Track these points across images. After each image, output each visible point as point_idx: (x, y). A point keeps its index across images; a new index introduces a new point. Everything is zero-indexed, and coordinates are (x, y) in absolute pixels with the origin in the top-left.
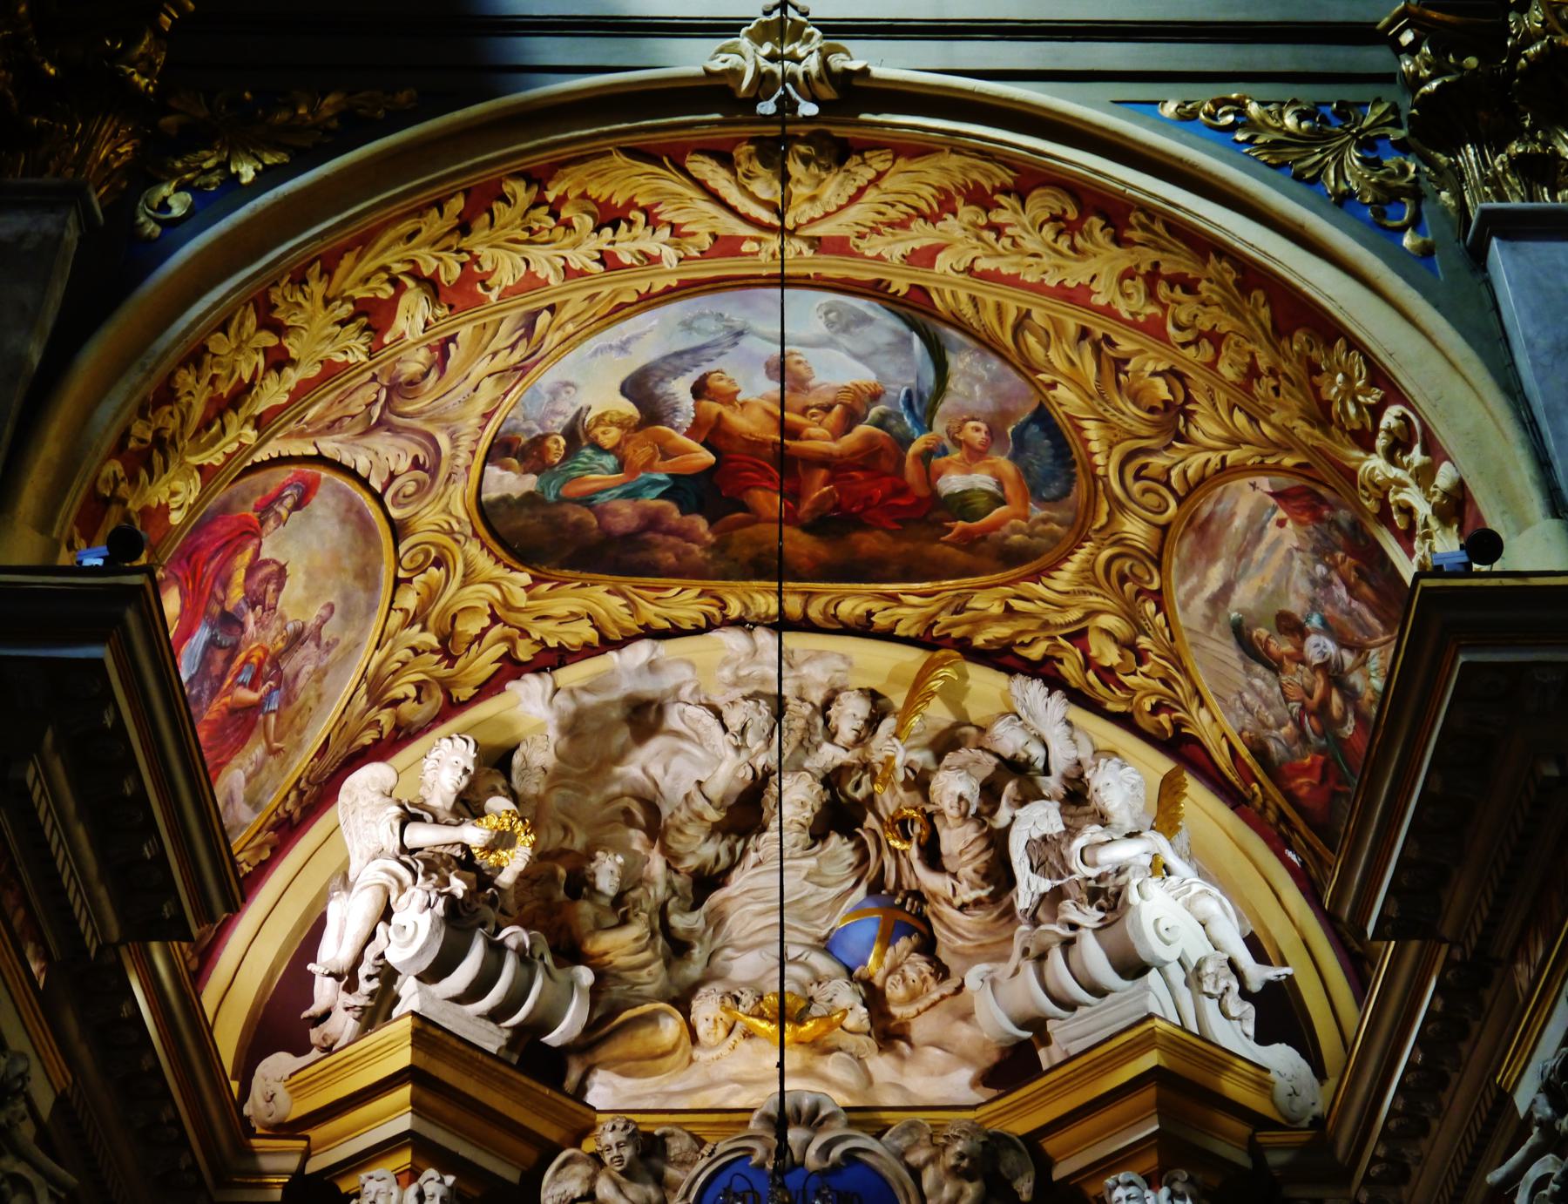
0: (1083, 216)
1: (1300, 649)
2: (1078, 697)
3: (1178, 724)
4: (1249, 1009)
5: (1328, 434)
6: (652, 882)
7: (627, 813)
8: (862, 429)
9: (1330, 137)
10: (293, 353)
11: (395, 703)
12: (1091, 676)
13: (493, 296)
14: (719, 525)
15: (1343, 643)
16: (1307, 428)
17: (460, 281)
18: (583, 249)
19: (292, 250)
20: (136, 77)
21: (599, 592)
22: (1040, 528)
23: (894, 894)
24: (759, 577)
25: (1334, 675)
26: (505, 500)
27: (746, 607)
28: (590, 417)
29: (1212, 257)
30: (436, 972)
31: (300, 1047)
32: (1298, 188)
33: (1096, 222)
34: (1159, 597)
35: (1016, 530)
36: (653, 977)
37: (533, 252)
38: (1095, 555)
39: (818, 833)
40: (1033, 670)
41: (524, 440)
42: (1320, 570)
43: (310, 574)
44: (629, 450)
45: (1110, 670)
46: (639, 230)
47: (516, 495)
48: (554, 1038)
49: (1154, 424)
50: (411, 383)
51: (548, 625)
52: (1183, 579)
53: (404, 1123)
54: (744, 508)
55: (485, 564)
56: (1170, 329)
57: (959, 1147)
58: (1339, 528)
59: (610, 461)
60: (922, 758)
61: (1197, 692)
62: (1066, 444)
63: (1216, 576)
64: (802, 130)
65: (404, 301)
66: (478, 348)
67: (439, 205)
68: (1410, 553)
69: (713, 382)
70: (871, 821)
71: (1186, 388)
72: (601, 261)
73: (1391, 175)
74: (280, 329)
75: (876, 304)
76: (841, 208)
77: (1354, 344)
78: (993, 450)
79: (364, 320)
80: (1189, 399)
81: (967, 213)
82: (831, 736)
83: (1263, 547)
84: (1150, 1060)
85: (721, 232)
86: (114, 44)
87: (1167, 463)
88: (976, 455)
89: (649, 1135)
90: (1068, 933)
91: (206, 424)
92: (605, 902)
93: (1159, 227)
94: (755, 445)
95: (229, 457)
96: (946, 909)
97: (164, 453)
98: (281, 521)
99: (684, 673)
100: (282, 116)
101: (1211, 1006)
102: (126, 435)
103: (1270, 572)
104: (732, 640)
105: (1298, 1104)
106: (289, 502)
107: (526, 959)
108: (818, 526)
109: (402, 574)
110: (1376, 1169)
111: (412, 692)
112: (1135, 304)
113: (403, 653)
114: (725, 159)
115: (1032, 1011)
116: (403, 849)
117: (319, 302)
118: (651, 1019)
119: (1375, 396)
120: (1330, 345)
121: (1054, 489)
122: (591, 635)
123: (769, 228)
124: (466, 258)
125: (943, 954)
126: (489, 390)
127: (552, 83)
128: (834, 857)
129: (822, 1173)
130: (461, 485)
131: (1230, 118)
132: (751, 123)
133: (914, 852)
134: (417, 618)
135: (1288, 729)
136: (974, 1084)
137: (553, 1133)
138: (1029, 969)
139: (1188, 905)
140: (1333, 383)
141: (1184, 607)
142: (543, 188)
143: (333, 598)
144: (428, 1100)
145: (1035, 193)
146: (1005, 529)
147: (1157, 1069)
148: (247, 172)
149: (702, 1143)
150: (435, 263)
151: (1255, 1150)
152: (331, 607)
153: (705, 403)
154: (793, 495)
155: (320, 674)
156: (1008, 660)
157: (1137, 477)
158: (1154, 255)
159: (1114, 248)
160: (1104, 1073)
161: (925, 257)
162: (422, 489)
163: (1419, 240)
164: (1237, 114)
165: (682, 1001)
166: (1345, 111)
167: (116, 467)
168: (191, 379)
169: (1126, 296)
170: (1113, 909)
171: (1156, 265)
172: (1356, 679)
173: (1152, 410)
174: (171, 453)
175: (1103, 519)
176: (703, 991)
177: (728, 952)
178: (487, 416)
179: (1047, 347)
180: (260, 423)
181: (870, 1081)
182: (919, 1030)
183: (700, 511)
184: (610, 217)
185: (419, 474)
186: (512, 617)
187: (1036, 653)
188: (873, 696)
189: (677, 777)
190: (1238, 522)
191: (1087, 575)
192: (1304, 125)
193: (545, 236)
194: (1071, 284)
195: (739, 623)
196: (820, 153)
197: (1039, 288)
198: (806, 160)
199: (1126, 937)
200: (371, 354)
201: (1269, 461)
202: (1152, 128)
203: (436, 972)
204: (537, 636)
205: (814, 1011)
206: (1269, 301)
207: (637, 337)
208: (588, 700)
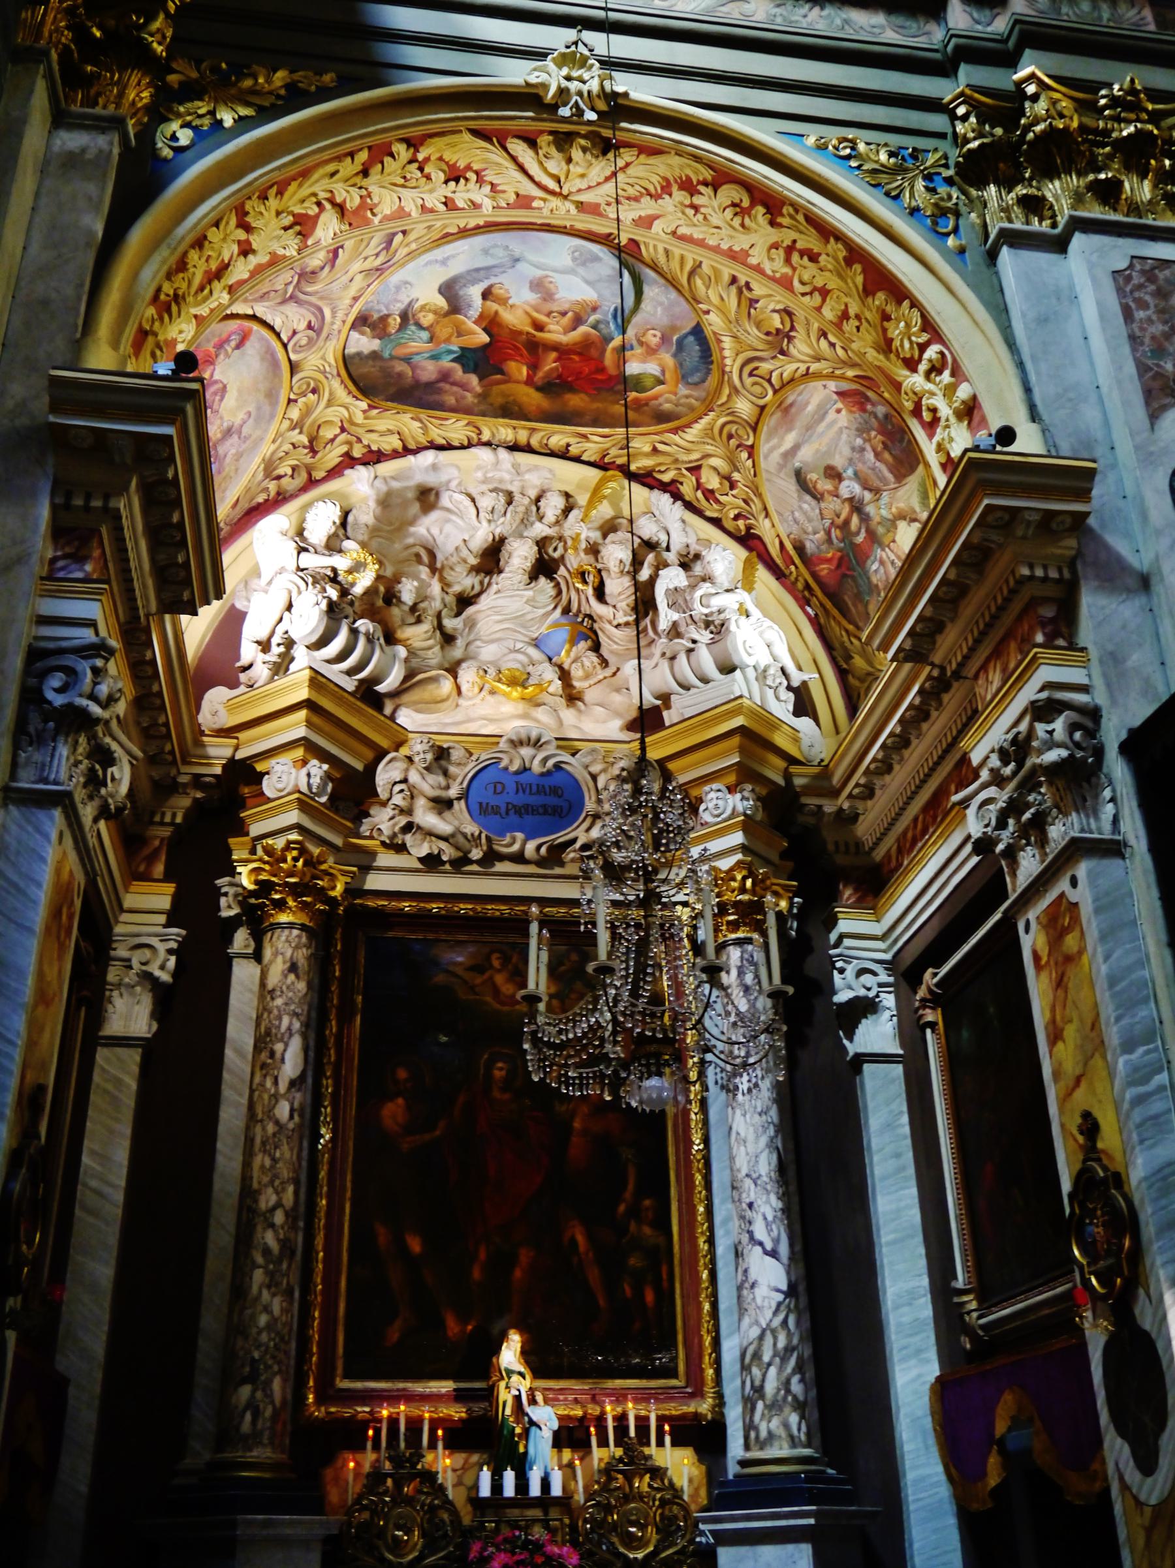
0: (753, 204)
1: (837, 488)
2: (689, 506)
3: (749, 528)
4: (791, 696)
5: (888, 359)
6: (434, 599)
7: (418, 556)
8: (583, 329)
9: (906, 170)
10: (254, 246)
11: (279, 477)
12: (699, 494)
13: (376, 220)
14: (486, 381)
15: (866, 487)
16: (875, 354)
17: (359, 207)
18: (435, 194)
19: (261, 176)
20: (155, 45)
21: (406, 418)
22: (683, 401)
23: (576, 615)
24: (504, 417)
25: (856, 506)
26: (359, 354)
27: (493, 435)
28: (417, 306)
29: (832, 240)
30: (322, 642)
31: (233, 684)
32: (888, 201)
33: (760, 210)
34: (751, 450)
35: (668, 401)
36: (434, 655)
37: (404, 193)
38: (715, 421)
39: (533, 577)
40: (664, 487)
41: (376, 316)
42: (859, 441)
43: (240, 391)
44: (437, 329)
45: (712, 492)
46: (472, 184)
47: (366, 351)
48: (382, 688)
49: (768, 343)
50: (313, 273)
51: (373, 436)
52: (768, 440)
53: (301, 732)
54: (502, 372)
55: (341, 394)
56: (796, 283)
57: (622, 764)
58: (876, 417)
59: (425, 335)
60: (595, 536)
61: (765, 509)
62: (709, 349)
63: (790, 440)
64: (583, 129)
65: (323, 218)
66: (356, 254)
67: (352, 155)
68: (931, 436)
69: (495, 291)
70: (562, 571)
71: (792, 321)
72: (445, 204)
73: (942, 199)
74: (248, 229)
75: (605, 249)
76: (599, 184)
77: (915, 304)
78: (662, 350)
79: (298, 228)
80: (792, 328)
81: (679, 196)
82: (541, 518)
83: (823, 424)
84: (739, 721)
85: (521, 192)
86: (138, 18)
87: (771, 367)
88: (651, 351)
89: (440, 748)
90: (692, 646)
91: (201, 289)
92: (406, 608)
93: (800, 218)
94: (517, 333)
95: (212, 310)
96: (608, 627)
97: (178, 304)
98: (228, 356)
99: (454, 473)
100: (248, 83)
101: (770, 693)
102: (159, 290)
103: (825, 440)
104: (484, 454)
105: (814, 751)
106: (233, 344)
107: (370, 639)
108: (548, 388)
109: (292, 396)
110: (857, 791)
111: (289, 472)
112: (776, 265)
113: (287, 447)
114: (532, 143)
115: (665, 689)
116: (299, 569)
117: (273, 213)
118: (434, 680)
119: (924, 337)
120: (899, 303)
121: (696, 378)
122: (398, 445)
123: (552, 193)
124: (364, 192)
125: (604, 651)
126: (359, 281)
128: (542, 591)
129: (542, 775)
130: (334, 342)
131: (848, 151)
132: (552, 121)
133: (590, 591)
134: (297, 425)
135: (821, 535)
136: (621, 730)
137: (384, 743)
138: (665, 665)
139: (761, 634)
140: (897, 327)
141: (766, 457)
142: (417, 151)
144: (316, 720)
145: (725, 187)
146: (661, 400)
147: (742, 727)
148: (227, 118)
149: (471, 754)
150: (345, 194)
151: (788, 776)
152: (249, 414)
153: (489, 303)
154: (534, 367)
155: (239, 456)
156: (649, 480)
157: (751, 374)
158: (793, 235)
159: (769, 227)
160: (709, 727)
161: (647, 222)
162: (311, 342)
163: (958, 243)
164: (853, 149)
165: (453, 670)
166: (916, 154)
167: (151, 311)
168: (196, 257)
169: (771, 259)
170: (719, 633)
171: (794, 241)
172: (870, 509)
173: (768, 334)
174: (183, 305)
175: (724, 399)
176: (464, 665)
177: (478, 643)
178: (356, 299)
179: (708, 288)
180: (231, 289)
181: (560, 722)
182: (589, 696)
183: (475, 371)
184: (455, 176)
185: (310, 332)
186: (353, 429)
187: (666, 478)
188: (567, 495)
189: (447, 536)
190: (811, 408)
191: (708, 432)
192: (892, 160)
193: (413, 183)
194: (736, 248)
195: (488, 444)
196: (594, 145)
197: (716, 249)
198: (584, 150)
199: (726, 650)
200: (299, 251)
201: (838, 372)
202: (801, 151)
203: (322, 642)
204: (365, 442)
205: (531, 681)
206: (864, 271)
207: (453, 256)
208: (396, 485)
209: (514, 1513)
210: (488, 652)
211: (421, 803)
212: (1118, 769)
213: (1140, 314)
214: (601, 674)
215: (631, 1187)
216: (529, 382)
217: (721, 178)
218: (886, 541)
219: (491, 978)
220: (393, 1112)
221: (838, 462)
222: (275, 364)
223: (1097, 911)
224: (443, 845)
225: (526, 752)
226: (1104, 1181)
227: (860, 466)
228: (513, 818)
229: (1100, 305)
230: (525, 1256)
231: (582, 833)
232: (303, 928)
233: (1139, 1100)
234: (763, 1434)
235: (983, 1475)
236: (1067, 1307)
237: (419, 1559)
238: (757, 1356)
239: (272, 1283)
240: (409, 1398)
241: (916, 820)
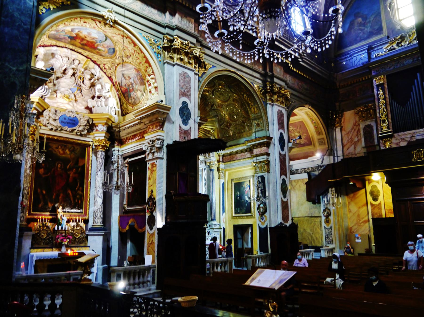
2: (101, 69)
3: (111, 76)
12: (103, 68)
34: (116, 67)
40: (97, 65)
82: (74, 64)
84: (108, 117)
88: (104, 47)
96: (84, 89)
114: (100, 22)
115: (94, 106)
133: (82, 82)
137: (46, 108)
148: (52, 7)
151: (112, 124)
172: (134, 86)
195: (67, 48)
208: (48, 52)
209: (61, 232)
210: (62, 89)
211: (51, 119)
212: (165, 149)
213: (181, 81)
214: (82, 98)
215: (78, 185)
216: (80, 43)
217: (128, 37)
218: (135, 92)
219: (59, 150)
221: (131, 76)
223: (159, 166)
224: (54, 127)
225: (71, 113)
226: (153, 199)
227: (134, 79)
229: (177, 79)
230: (61, 195)
233: (159, 190)
234: (97, 222)
235: (125, 228)
236: (144, 210)
237: (46, 237)
238: (97, 212)
240: (44, 215)
241: (131, 136)
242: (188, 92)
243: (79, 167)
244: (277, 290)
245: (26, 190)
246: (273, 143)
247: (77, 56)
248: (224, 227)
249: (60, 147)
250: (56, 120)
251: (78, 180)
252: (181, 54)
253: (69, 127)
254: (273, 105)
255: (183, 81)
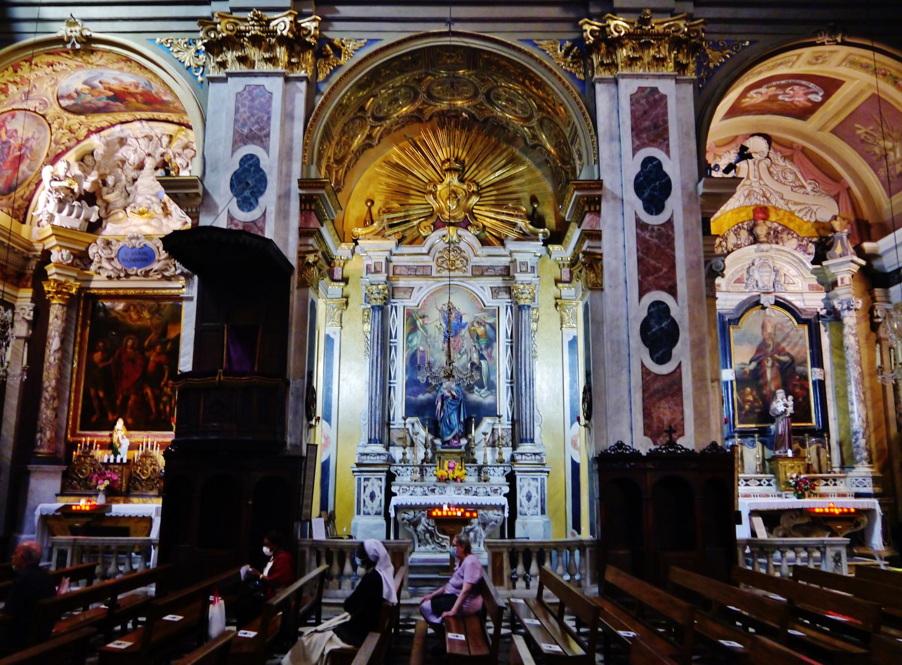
36: (121, 202)
118: (117, 213)
127: (27, 38)
143: (34, 130)
144: (59, 238)
208: (108, 139)
211: (103, 260)
220: (97, 356)
222: (35, 117)
225: (133, 241)
228: (133, 263)
230: (133, 397)
231: (156, 266)
232: (60, 304)
239: (47, 407)
240: (90, 436)
242: (262, 129)
243: (169, 340)
244: (594, 655)
245: (47, 391)
246: (615, 197)
247: (163, 128)
248: (577, 460)
249: (132, 308)
250: (113, 259)
251: (166, 367)
252: (243, 47)
253: (139, 267)
254: (616, 82)
255: (246, 109)
